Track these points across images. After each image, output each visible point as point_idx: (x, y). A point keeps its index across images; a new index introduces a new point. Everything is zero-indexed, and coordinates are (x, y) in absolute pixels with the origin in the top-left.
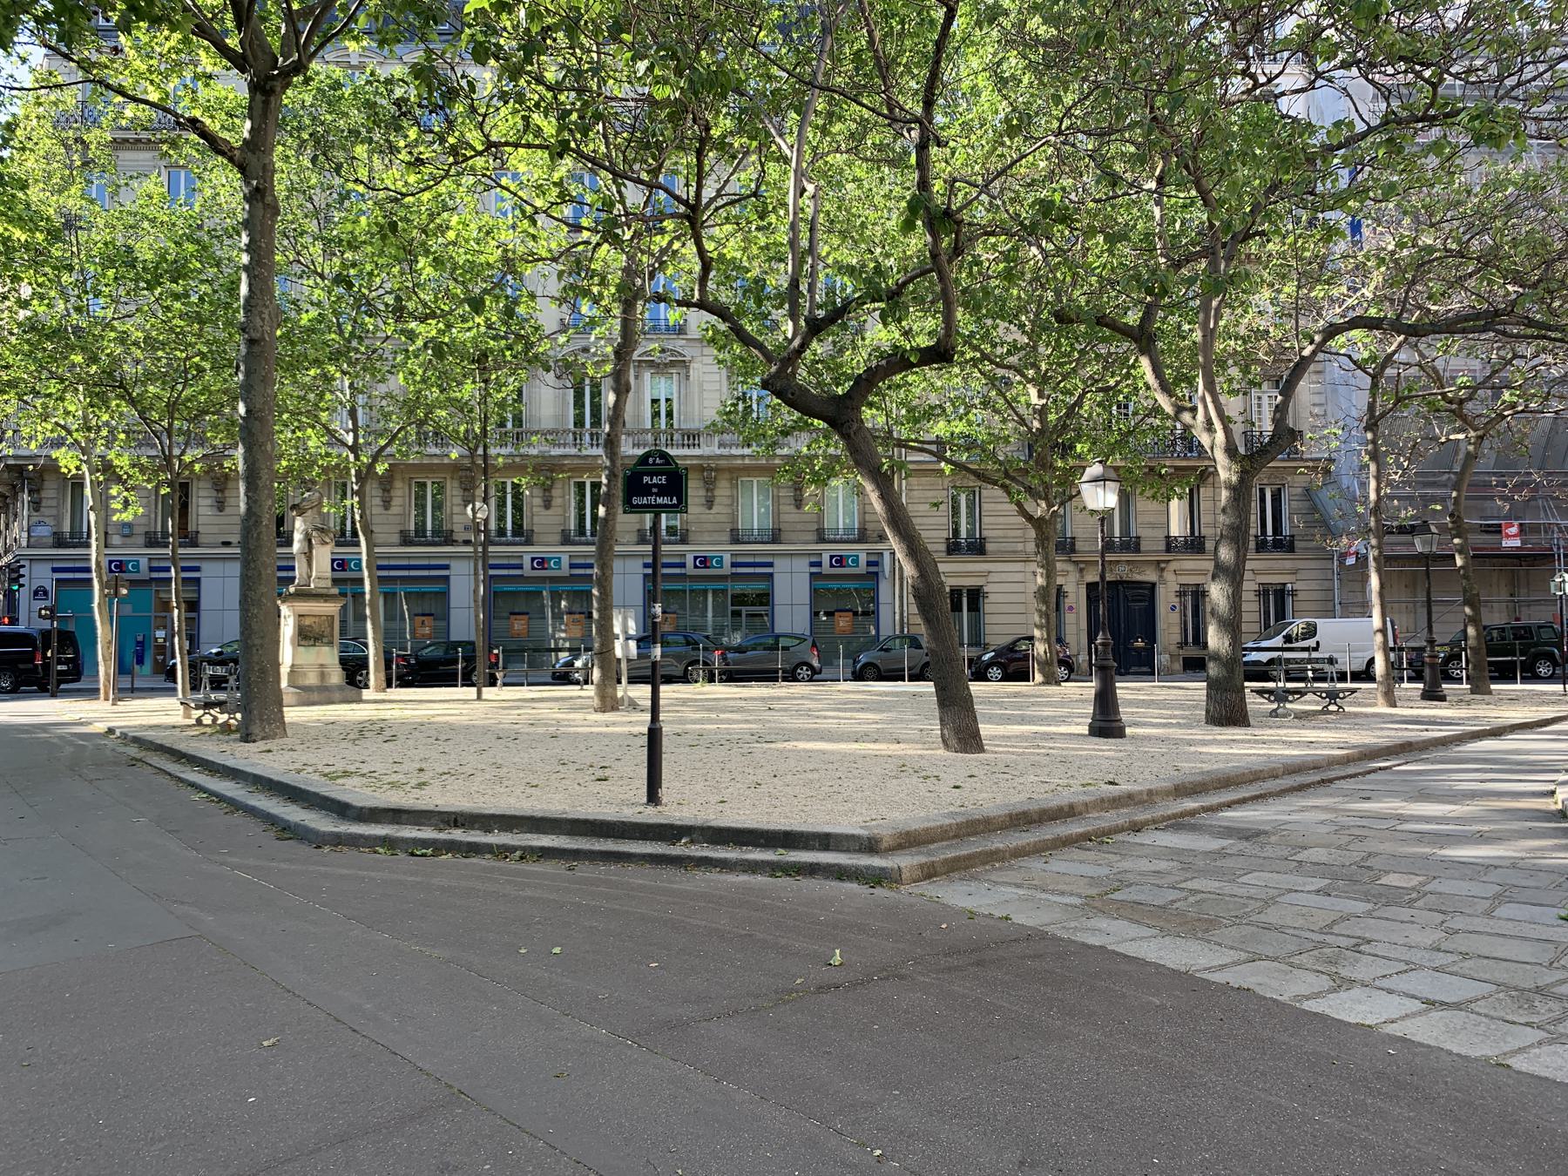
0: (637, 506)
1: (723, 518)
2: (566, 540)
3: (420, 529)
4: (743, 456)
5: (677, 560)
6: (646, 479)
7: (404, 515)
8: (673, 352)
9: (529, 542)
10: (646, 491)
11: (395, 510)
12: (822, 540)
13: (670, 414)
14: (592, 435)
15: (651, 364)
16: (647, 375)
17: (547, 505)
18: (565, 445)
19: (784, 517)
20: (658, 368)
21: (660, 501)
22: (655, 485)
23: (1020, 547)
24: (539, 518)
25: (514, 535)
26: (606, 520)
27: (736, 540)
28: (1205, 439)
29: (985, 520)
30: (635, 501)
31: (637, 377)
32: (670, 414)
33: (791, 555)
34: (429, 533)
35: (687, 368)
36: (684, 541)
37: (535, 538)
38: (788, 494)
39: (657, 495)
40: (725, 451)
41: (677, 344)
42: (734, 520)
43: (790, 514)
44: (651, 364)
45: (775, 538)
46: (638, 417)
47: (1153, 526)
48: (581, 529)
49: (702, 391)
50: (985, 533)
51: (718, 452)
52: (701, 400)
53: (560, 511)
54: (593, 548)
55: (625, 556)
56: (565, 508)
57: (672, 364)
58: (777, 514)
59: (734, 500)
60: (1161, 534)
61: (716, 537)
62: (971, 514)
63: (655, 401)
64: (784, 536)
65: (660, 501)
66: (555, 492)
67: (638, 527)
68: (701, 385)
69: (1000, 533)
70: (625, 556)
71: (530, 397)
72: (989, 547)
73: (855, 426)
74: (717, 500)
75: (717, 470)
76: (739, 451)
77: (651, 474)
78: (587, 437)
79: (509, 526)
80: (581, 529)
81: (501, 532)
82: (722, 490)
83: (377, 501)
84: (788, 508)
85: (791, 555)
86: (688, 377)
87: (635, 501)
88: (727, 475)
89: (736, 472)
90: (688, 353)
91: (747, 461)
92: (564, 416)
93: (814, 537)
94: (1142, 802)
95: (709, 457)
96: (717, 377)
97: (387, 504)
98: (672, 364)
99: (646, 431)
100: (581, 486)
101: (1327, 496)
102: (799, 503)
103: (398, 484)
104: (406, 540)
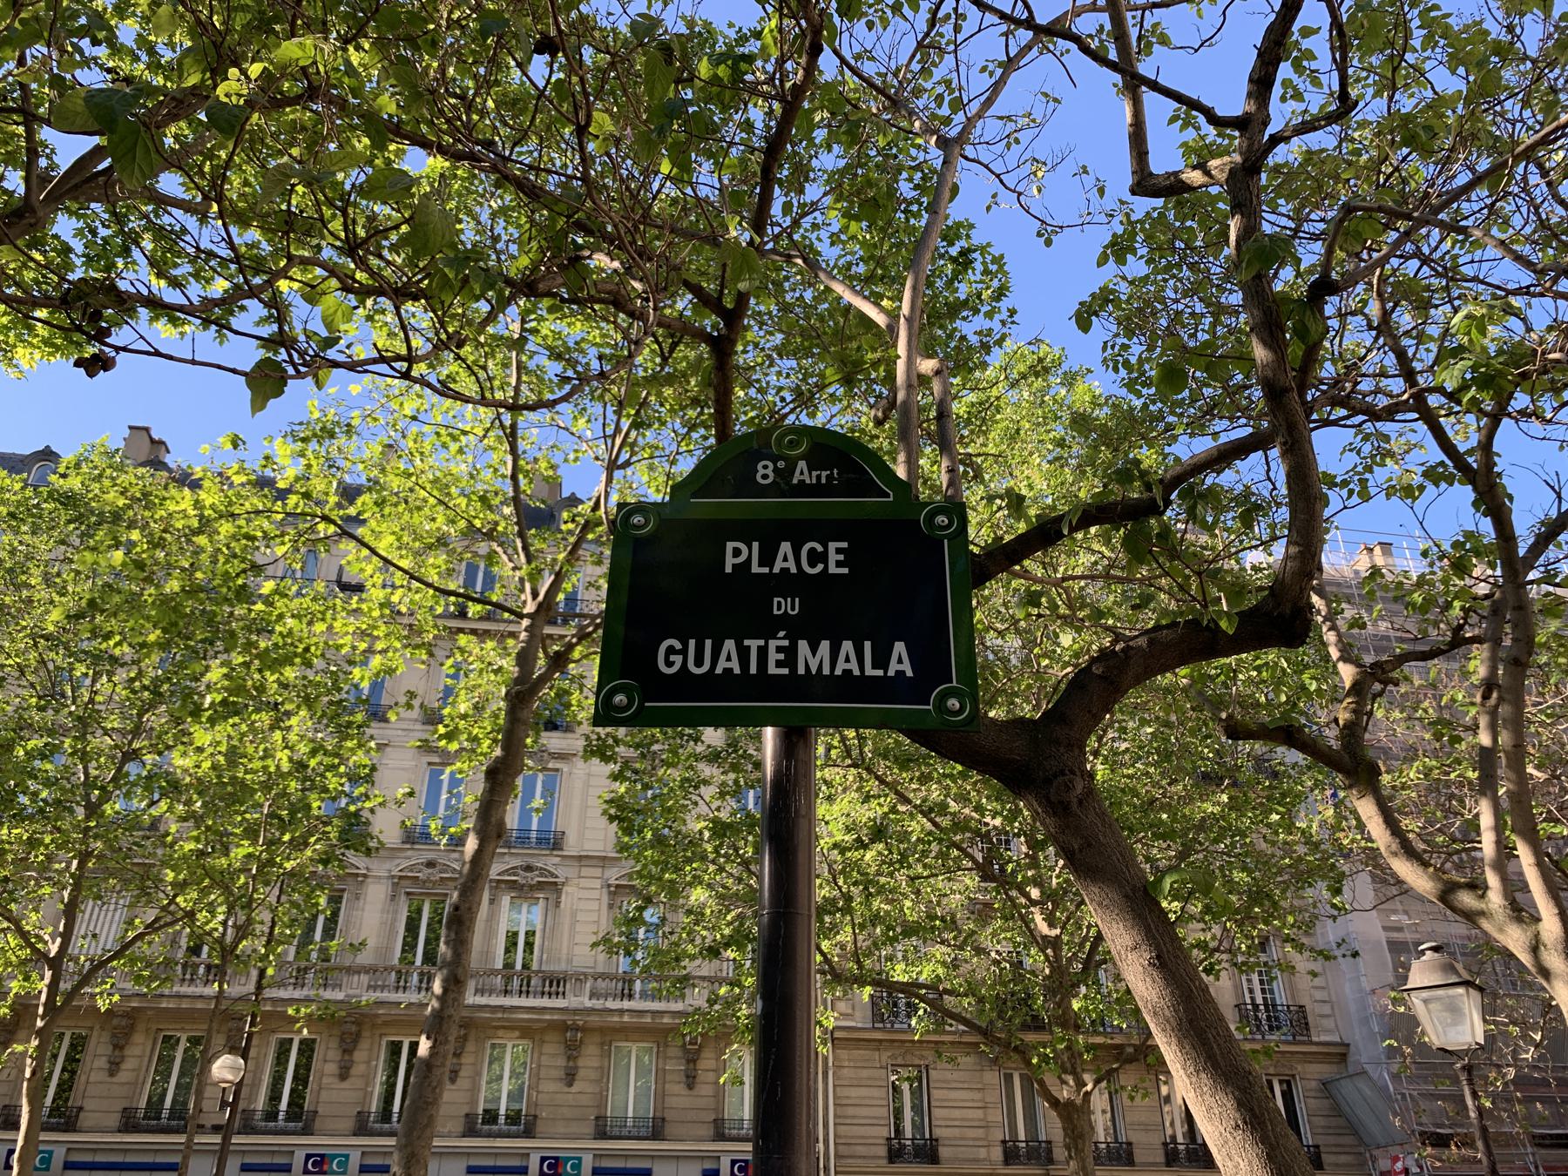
0: (684, 685)
1: (585, 1100)
2: (362, 1129)
3: (155, 1105)
4: (621, 1012)
5: (515, 1162)
6: (736, 554)
7: (136, 1085)
8: (543, 871)
9: (307, 1131)
10: (741, 607)
11: (124, 1076)
12: (720, 1136)
13: (529, 945)
14: (421, 974)
15: (513, 885)
16: (506, 900)
17: (344, 1075)
18: (383, 988)
19: (671, 1102)
20: (523, 891)
21: (813, 658)
22: (787, 583)
23: (983, 1153)
24: (332, 1095)
25: (287, 1120)
26: (428, 1064)
27: (601, 1134)
28: (1514, 939)
29: (936, 1112)
30: (671, 656)
31: (492, 901)
32: (529, 945)
33: (678, 1157)
34: (165, 1114)
35: (559, 892)
36: (529, 1133)
37: (318, 1124)
38: (676, 1066)
39: (808, 628)
40: (597, 1004)
41: (550, 862)
42: (602, 1102)
43: (678, 1097)
44: (513, 885)
45: (657, 1134)
46: (488, 954)
47: (1146, 1128)
48: (386, 1115)
49: (574, 922)
50: (937, 1132)
51: (588, 1004)
52: (572, 936)
53: (359, 1083)
54: (392, 1141)
55: (444, 1154)
56: (368, 1079)
57: (540, 886)
58: (661, 1095)
59: (604, 1073)
60: (1157, 1140)
61: (575, 1128)
62: (917, 1109)
63: (512, 938)
64: (669, 1130)
65: (813, 658)
66: (359, 1056)
67: (466, 1110)
68: (574, 914)
69: (956, 1132)
70: (444, 1154)
71: (347, 922)
72: (944, 1152)
73: (1079, 787)
74: (581, 1073)
75: (583, 1029)
76: (612, 1004)
77: (768, 535)
78: (415, 977)
79: (283, 1105)
80: (386, 1115)
81: (271, 1115)
82: (589, 1060)
83: (102, 1063)
84: (676, 1088)
85: (678, 1157)
86: (558, 904)
87: (671, 656)
88: (597, 1038)
89: (611, 1033)
90: (562, 873)
91: (626, 1019)
92: (389, 949)
93: (709, 1131)
94: (72, 1078)
95: (576, 1011)
96: (595, 906)
97: (114, 1067)
98: (540, 886)
99: (494, 972)
100: (395, 1049)
101: (1349, 1091)
102: (691, 1080)
103: (138, 1038)
104: (129, 1123)
